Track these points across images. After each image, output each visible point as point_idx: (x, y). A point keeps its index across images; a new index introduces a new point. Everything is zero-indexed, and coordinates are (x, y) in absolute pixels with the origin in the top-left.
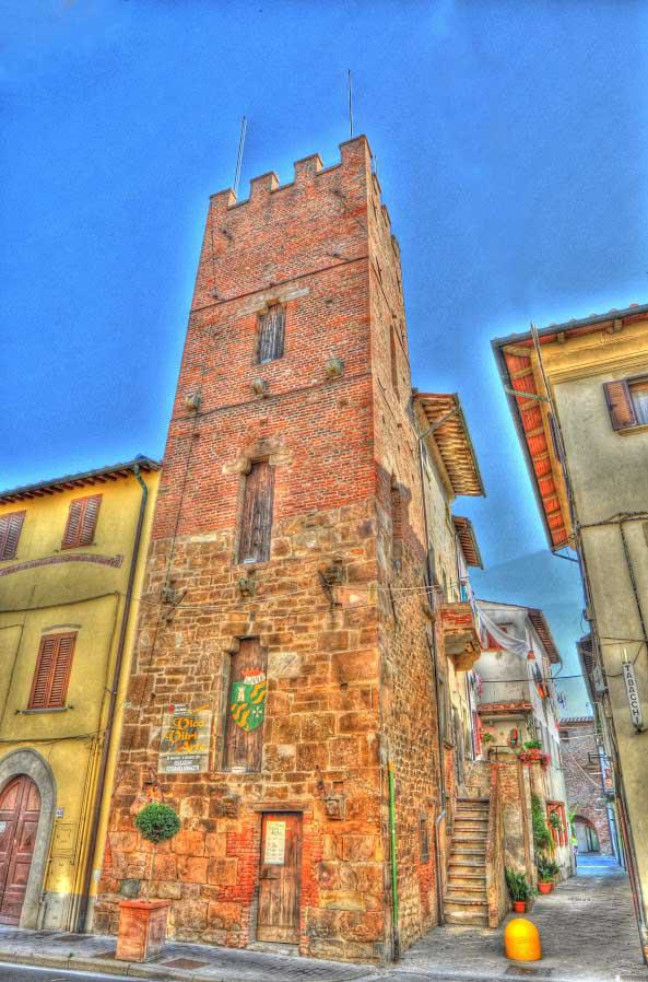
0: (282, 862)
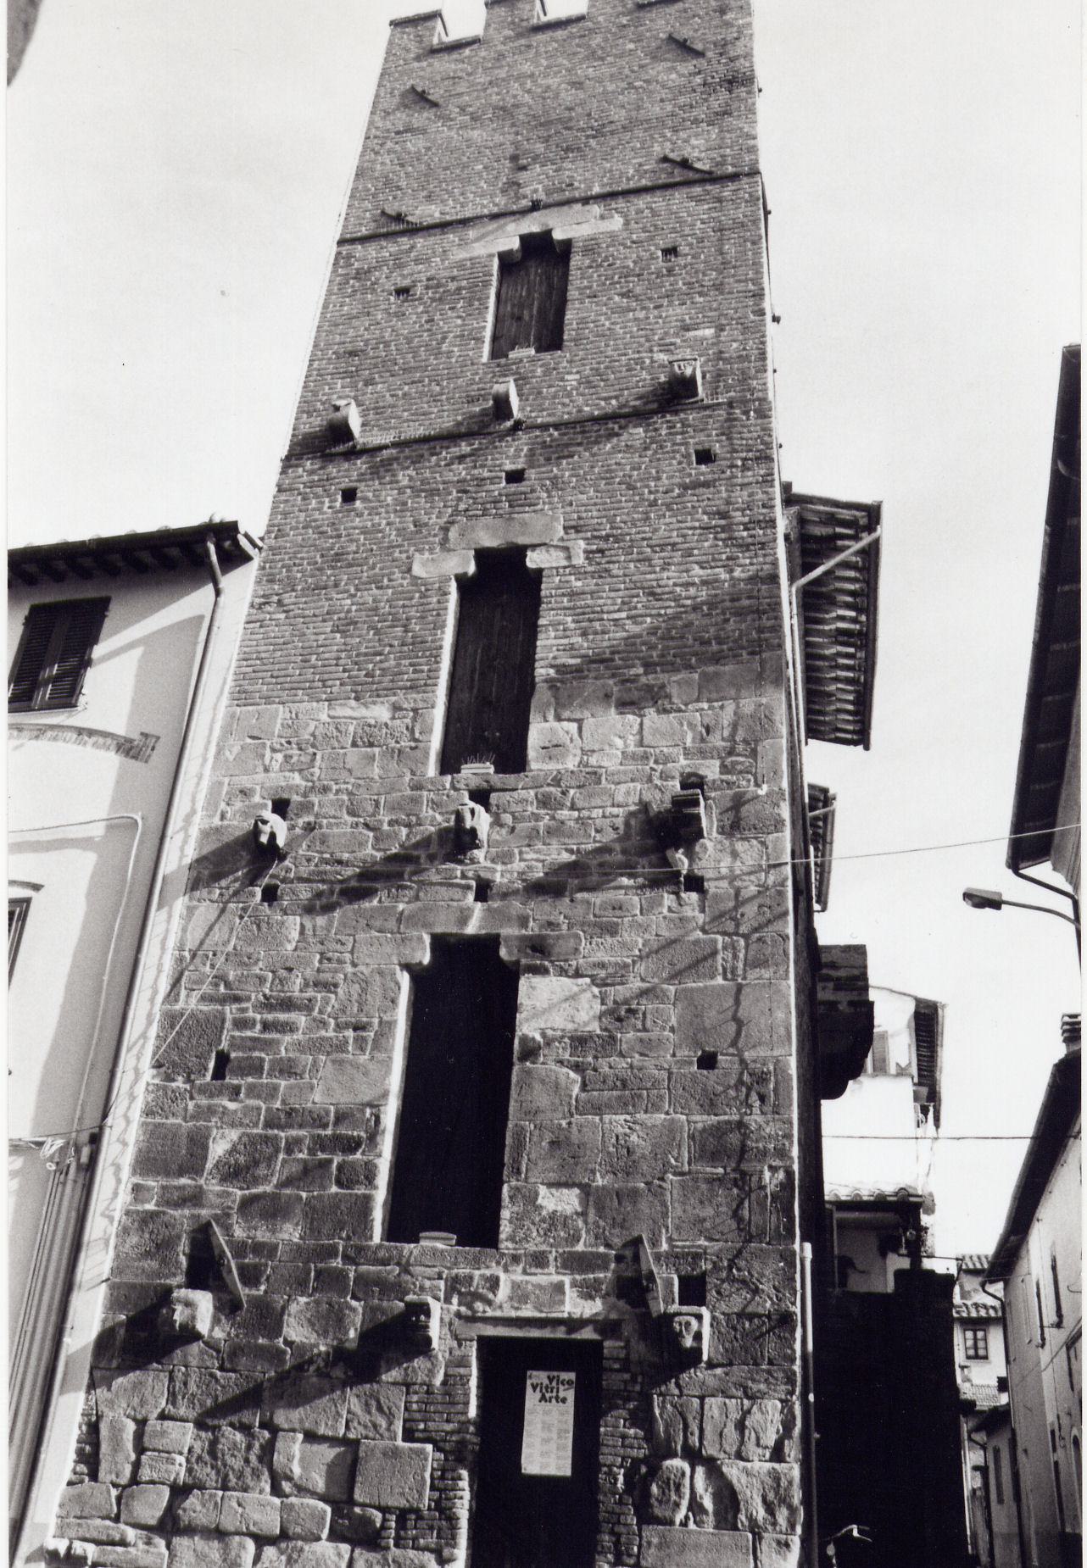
0: (524, 983)
